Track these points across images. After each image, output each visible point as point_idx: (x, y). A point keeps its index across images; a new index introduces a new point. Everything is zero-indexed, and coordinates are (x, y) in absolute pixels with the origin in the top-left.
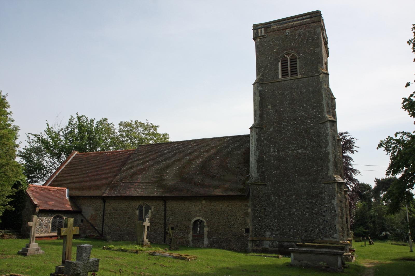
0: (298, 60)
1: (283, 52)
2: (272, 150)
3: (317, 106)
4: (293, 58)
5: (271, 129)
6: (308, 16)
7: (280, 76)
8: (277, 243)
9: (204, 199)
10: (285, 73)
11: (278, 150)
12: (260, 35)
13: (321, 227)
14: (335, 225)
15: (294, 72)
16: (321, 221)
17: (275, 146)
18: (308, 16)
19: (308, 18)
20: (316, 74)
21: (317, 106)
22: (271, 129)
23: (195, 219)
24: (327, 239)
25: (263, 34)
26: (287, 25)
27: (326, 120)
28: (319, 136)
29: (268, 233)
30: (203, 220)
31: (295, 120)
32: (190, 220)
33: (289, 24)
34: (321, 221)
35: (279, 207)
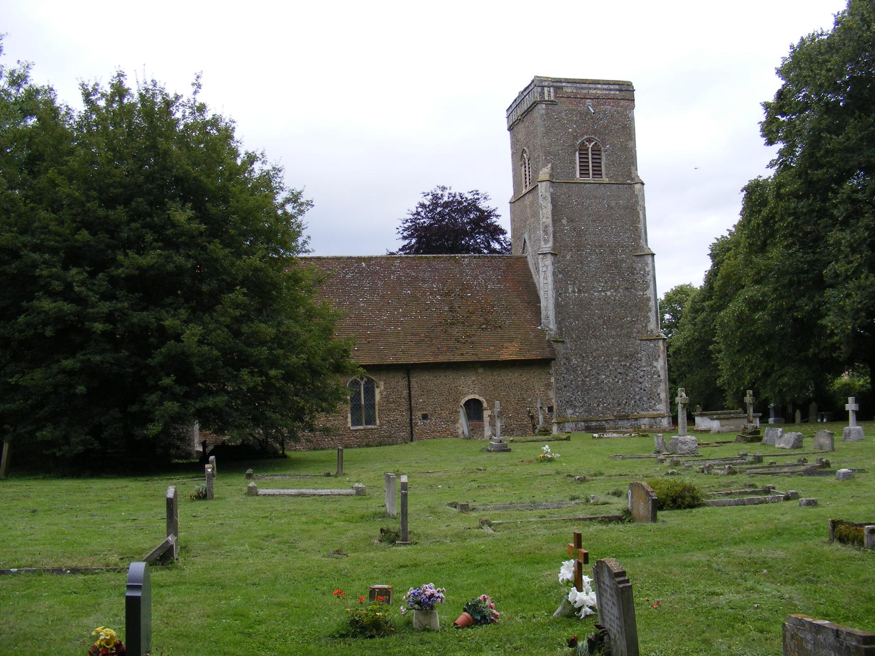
0: (603, 154)
1: (582, 136)
2: (570, 290)
3: (630, 230)
4: (595, 148)
5: (568, 257)
6: (617, 87)
7: (578, 175)
8: (583, 424)
9: (481, 367)
10: (584, 171)
11: (579, 291)
12: (546, 98)
13: (637, 397)
14: (658, 394)
15: (597, 172)
16: (637, 389)
17: (574, 283)
18: (617, 87)
19: (617, 90)
20: (629, 181)
21: (630, 230)
22: (568, 257)
23: (466, 399)
24: (644, 413)
25: (552, 98)
26: (586, 91)
27: (646, 252)
28: (633, 274)
29: (570, 411)
30: (481, 399)
31: (601, 246)
32: (456, 401)
33: (591, 91)
34: (637, 389)
35: (582, 373)
